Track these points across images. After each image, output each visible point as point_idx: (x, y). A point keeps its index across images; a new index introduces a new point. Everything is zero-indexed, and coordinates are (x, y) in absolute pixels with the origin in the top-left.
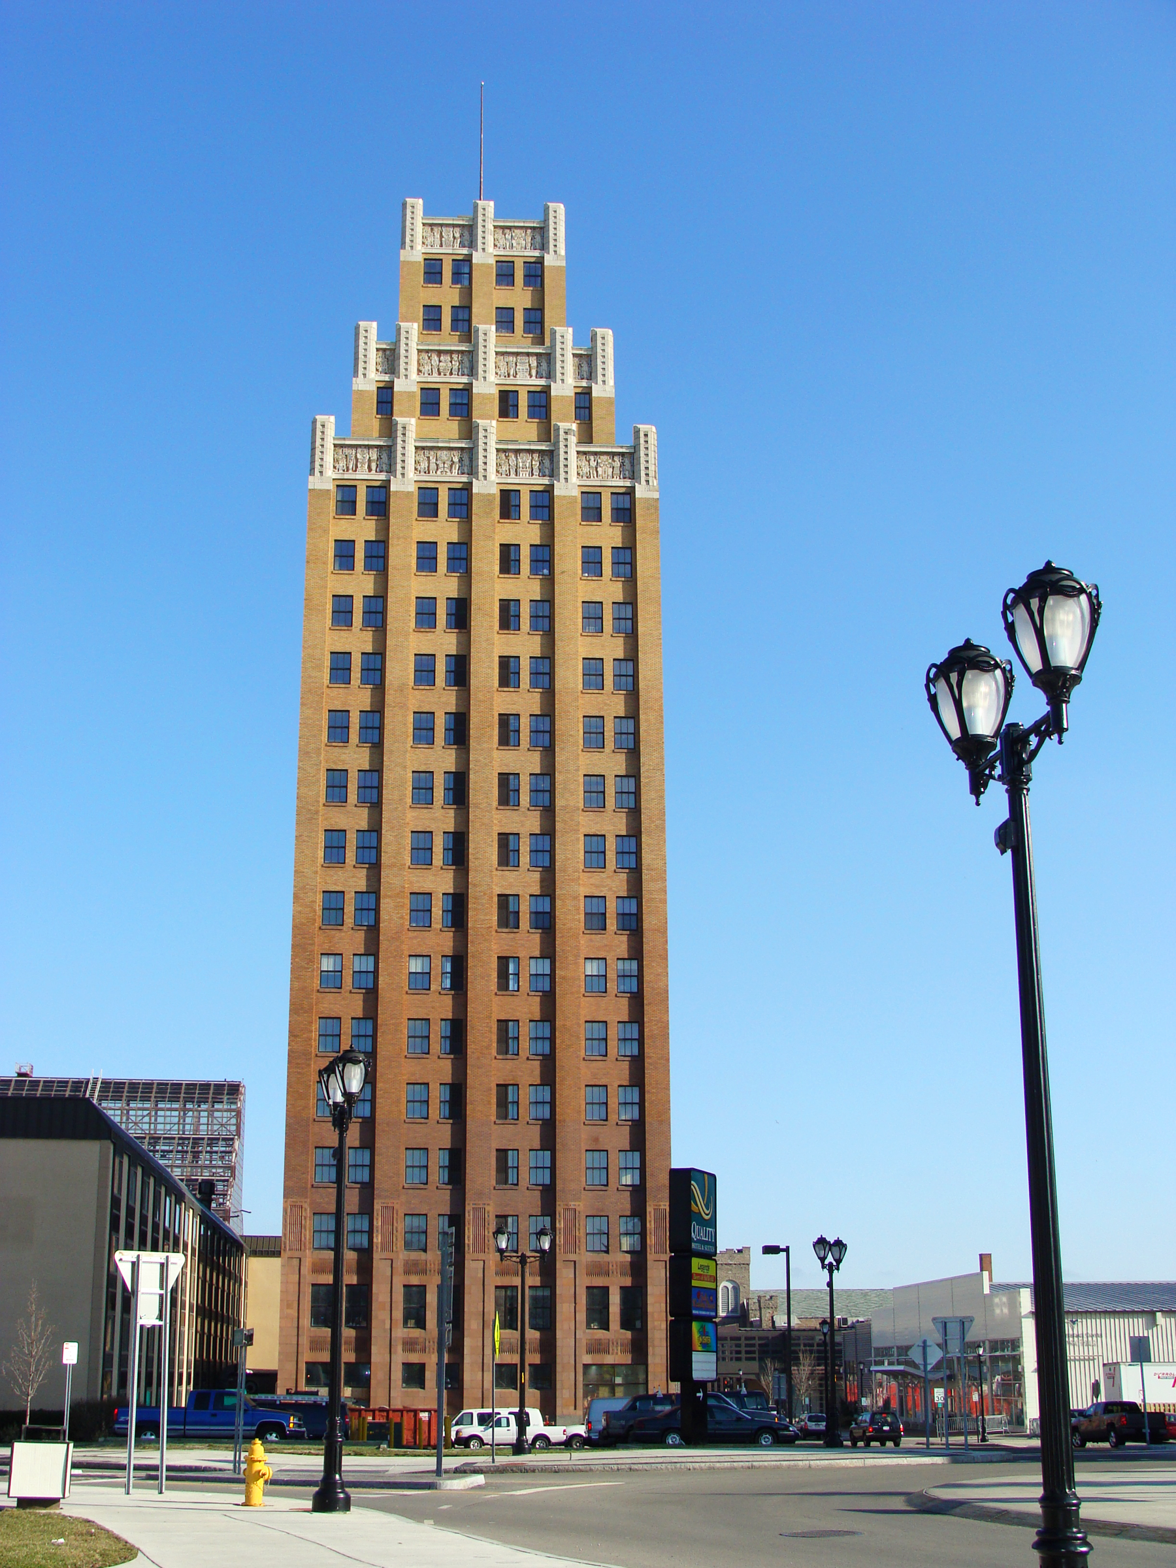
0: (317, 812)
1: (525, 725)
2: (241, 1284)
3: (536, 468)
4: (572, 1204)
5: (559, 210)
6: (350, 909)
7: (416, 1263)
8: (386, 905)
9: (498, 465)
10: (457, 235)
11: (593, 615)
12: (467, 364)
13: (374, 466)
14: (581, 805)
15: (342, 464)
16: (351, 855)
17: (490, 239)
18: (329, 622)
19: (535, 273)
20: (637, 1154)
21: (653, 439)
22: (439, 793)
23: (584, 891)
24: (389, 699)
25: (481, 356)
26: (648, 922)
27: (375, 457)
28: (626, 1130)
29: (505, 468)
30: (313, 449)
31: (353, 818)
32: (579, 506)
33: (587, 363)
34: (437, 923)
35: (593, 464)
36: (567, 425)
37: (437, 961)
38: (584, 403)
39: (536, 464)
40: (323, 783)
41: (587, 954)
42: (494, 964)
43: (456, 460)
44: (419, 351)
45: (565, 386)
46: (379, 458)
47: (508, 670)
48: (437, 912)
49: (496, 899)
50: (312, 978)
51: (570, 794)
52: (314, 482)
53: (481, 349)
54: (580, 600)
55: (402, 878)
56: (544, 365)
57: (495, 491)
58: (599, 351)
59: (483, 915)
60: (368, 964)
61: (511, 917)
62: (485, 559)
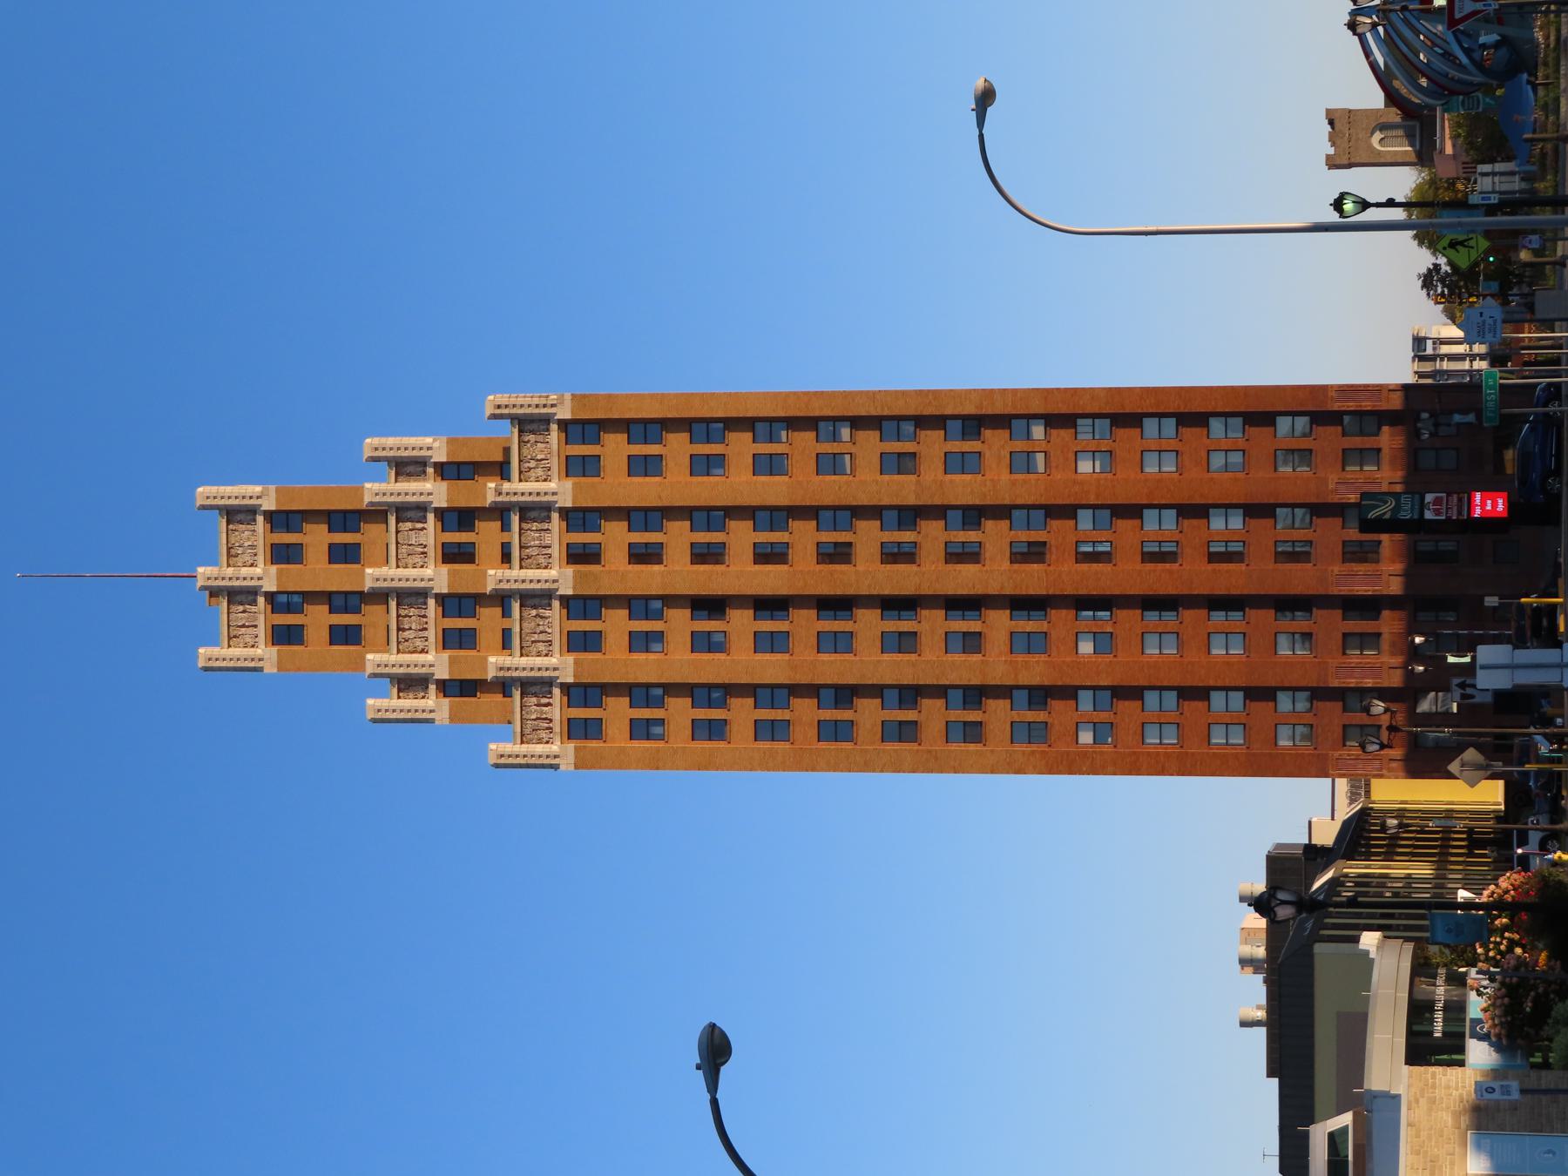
2: (1405, 810)
3: (540, 526)
5: (203, 492)
8: (1024, 679)
9: (539, 567)
10: (241, 608)
11: (705, 465)
12: (413, 600)
13: (544, 701)
14: (913, 478)
15: (544, 735)
17: (245, 571)
18: (722, 744)
19: (280, 520)
21: (503, 399)
22: (906, 626)
23: (1005, 476)
25: (403, 584)
27: (534, 700)
28: (1254, 431)
29: (542, 560)
33: (406, 467)
35: (533, 464)
36: (490, 491)
37: (1082, 625)
38: (446, 471)
39: (535, 526)
40: (897, 746)
42: (1085, 567)
43: (534, 612)
44: (399, 651)
45: (434, 491)
46: (535, 695)
48: (1030, 626)
49: (1016, 566)
50: (1102, 753)
51: (902, 490)
52: (270, 668)
53: (395, 584)
55: (996, 663)
56: (409, 514)
57: (570, 571)
59: (1033, 579)
60: (1085, 698)
61: (1033, 549)
62: (648, 580)
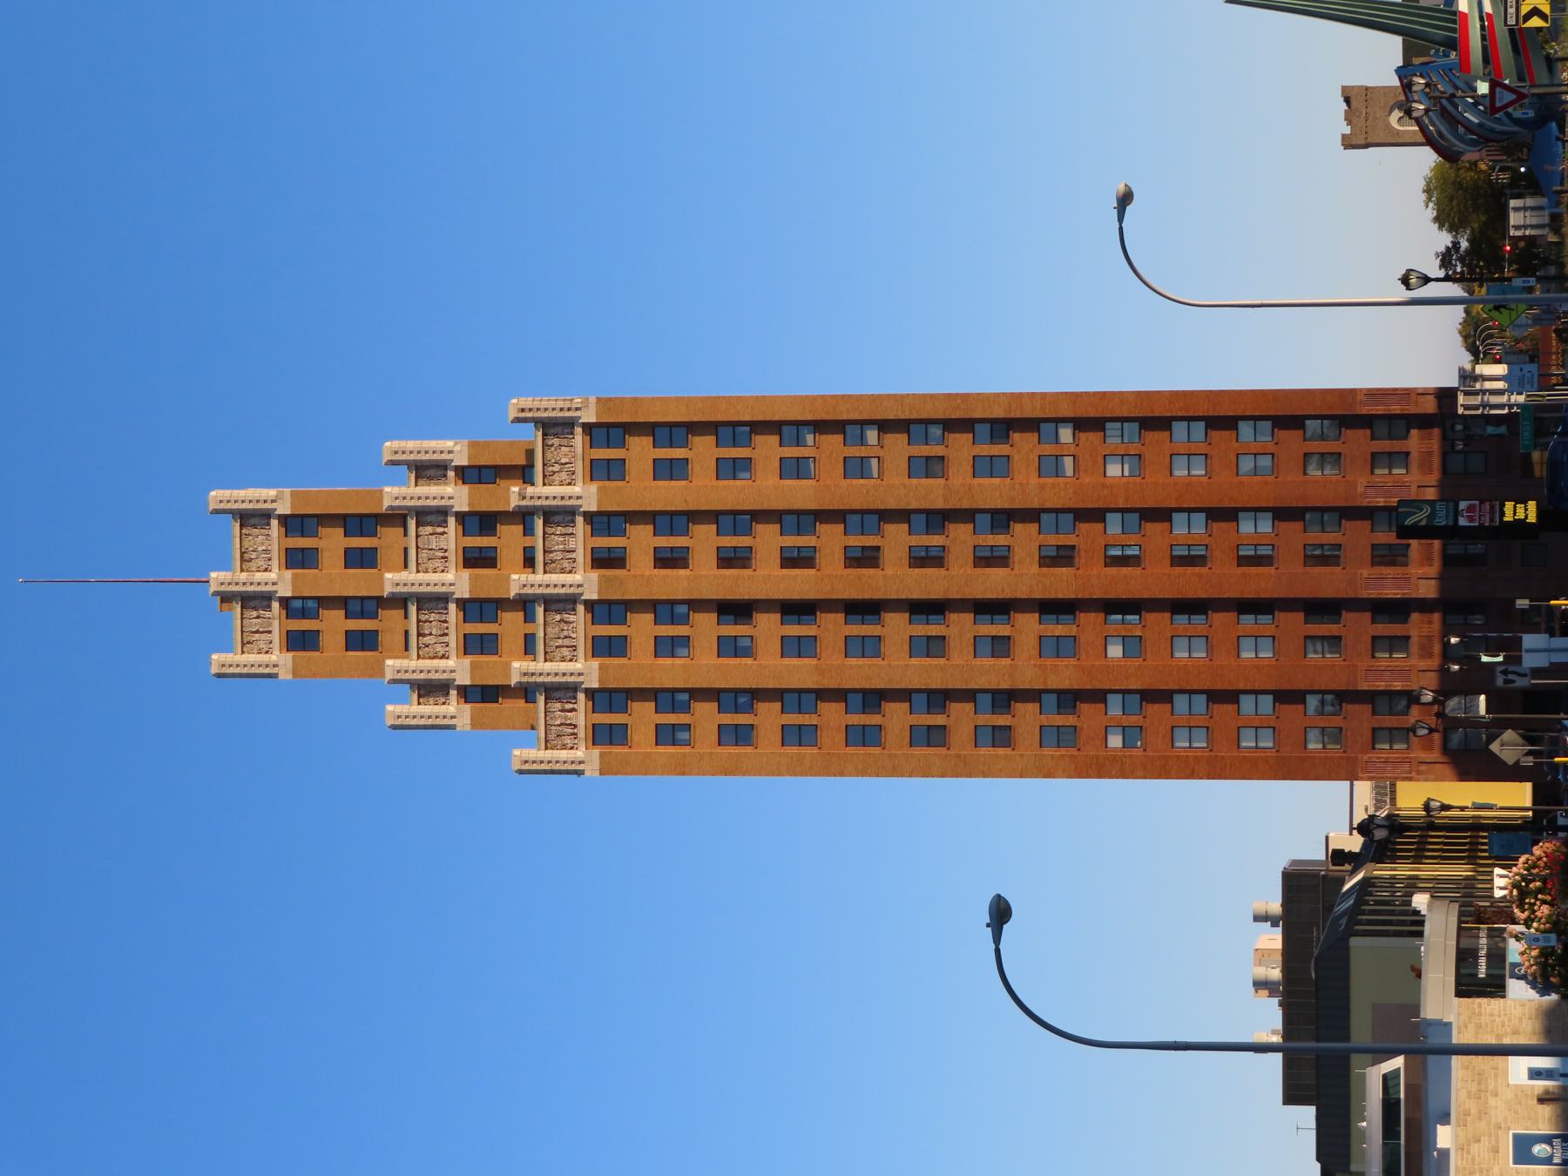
0: (958, 756)
1: (729, 541)
3: (564, 530)
4: (1360, 490)
6: (671, 719)
7: (1422, 647)
9: (563, 571)
10: (255, 614)
14: (941, 481)
15: (568, 741)
16: (743, 719)
17: (259, 576)
18: (749, 750)
20: (1108, 425)
22: (934, 630)
23: (1034, 480)
24: (833, 685)
26: (998, 413)
27: (559, 705)
29: (566, 564)
30: (553, 772)
31: (706, 717)
32: (607, 483)
33: (427, 470)
34: (1071, 630)
35: (557, 468)
36: (513, 495)
37: (1111, 629)
39: (559, 530)
41: (893, 481)
42: (1113, 570)
43: (558, 617)
45: (455, 495)
47: (731, 559)
49: (1045, 570)
54: (715, 482)
58: (412, 457)
62: (674, 584)
